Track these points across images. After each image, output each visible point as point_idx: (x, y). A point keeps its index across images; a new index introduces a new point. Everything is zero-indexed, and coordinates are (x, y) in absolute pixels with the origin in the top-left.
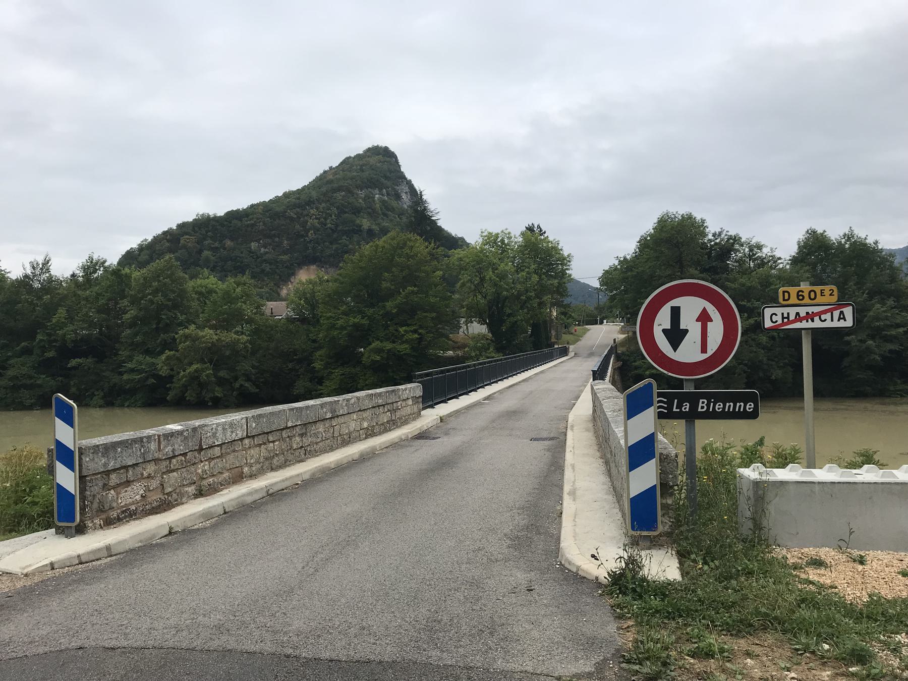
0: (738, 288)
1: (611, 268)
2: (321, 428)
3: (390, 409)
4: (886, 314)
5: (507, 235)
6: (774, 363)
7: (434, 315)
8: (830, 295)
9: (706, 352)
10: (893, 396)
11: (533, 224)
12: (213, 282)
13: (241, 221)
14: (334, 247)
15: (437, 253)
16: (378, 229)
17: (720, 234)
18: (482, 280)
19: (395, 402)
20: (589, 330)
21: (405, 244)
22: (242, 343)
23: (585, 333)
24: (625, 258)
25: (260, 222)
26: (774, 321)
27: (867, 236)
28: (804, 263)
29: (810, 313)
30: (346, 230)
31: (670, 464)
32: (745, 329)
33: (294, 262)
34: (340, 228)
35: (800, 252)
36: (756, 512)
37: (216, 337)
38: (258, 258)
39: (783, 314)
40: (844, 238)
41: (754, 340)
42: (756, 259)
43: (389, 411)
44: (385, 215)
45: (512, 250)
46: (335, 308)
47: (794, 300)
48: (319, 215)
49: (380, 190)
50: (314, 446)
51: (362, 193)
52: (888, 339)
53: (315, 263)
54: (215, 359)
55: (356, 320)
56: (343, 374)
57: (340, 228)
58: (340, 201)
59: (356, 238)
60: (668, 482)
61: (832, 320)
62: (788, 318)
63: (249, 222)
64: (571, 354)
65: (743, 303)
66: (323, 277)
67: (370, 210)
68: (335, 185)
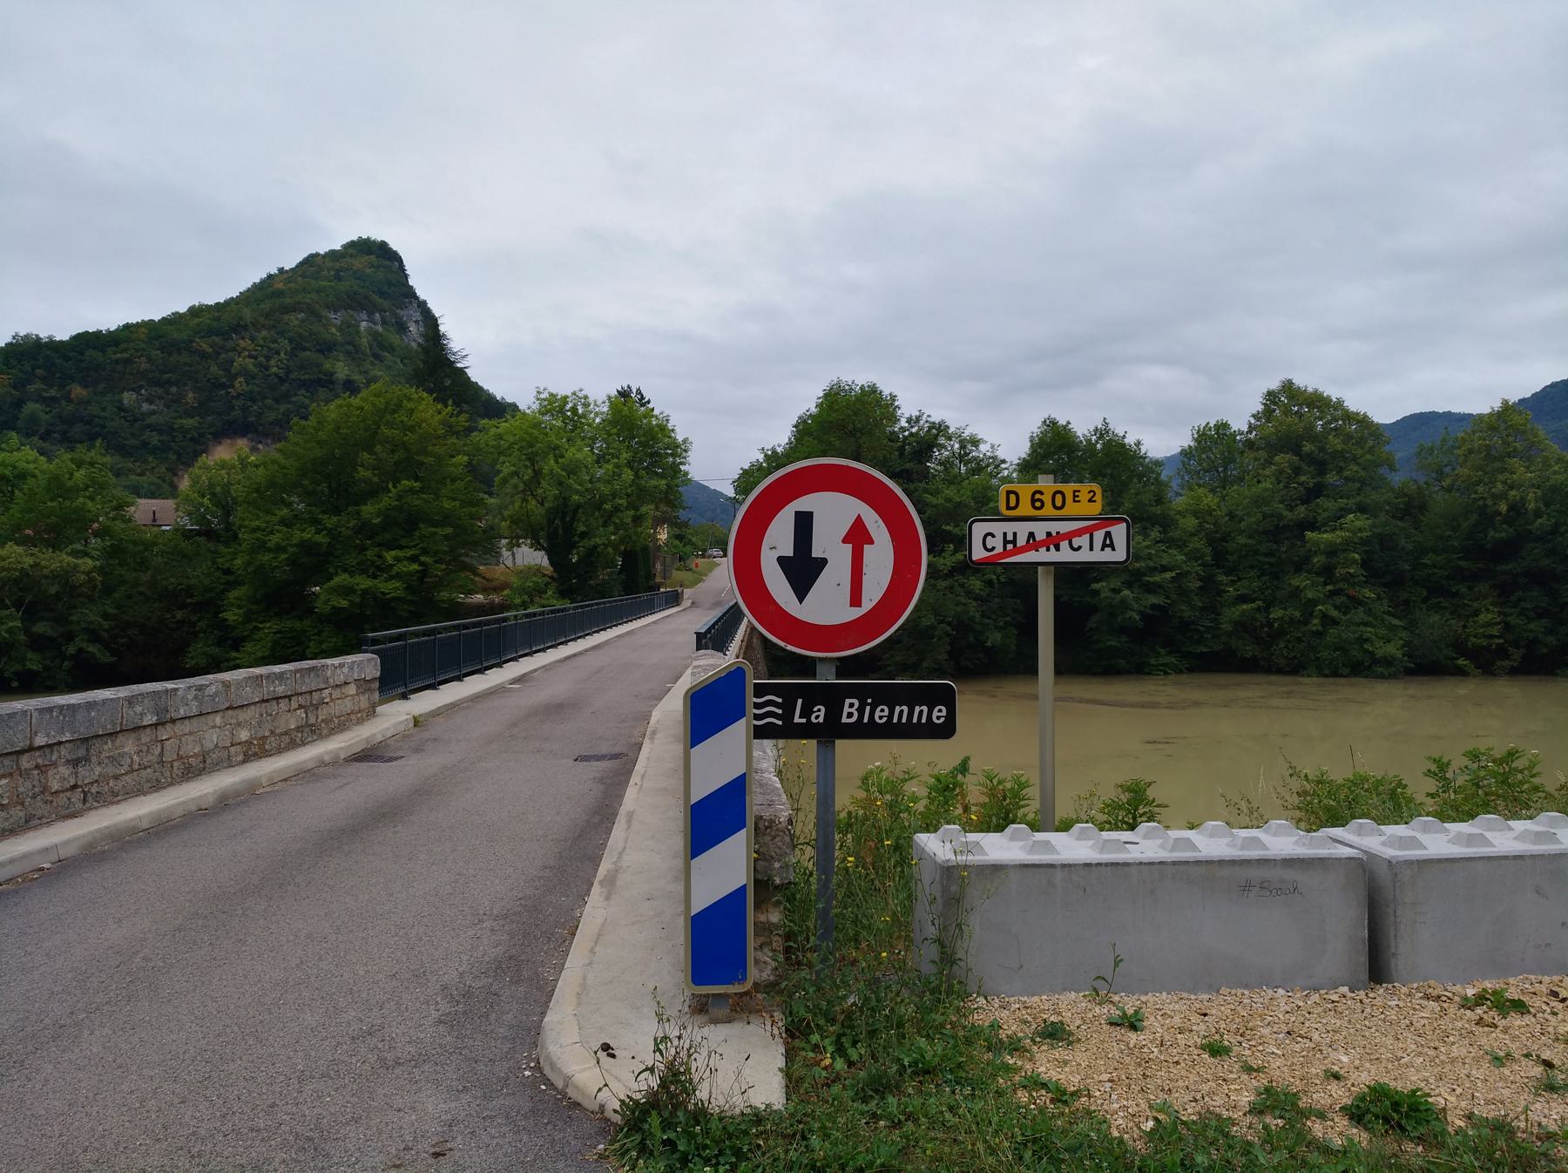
0: (942, 504)
1: (753, 465)
2: (129, 745)
3: (303, 703)
4: (1148, 551)
5: (583, 400)
6: (990, 621)
7: (449, 530)
8: (1090, 501)
9: (859, 605)
10: (1154, 673)
11: (629, 387)
12: (30, 458)
13: (104, 352)
14: (283, 408)
15: (457, 423)
16: (364, 381)
17: (918, 419)
18: (537, 474)
19: (315, 691)
20: (719, 565)
21: (399, 406)
22: (83, 572)
23: (710, 570)
24: (774, 452)
25: (142, 356)
26: (989, 547)
27: (1126, 432)
28: (1039, 469)
29: (1054, 534)
30: (305, 380)
31: (777, 840)
32: (950, 569)
33: (204, 430)
34: (294, 376)
35: (1033, 452)
36: (945, 928)
37: (30, 560)
38: (136, 420)
39: (1005, 534)
40: (1095, 434)
41: (962, 586)
42: (969, 461)
43: (301, 707)
44: (376, 356)
45: (589, 425)
46: (268, 512)
47: (1025, 509)
48: (256, 350)
49: (370, 314)
50: (108, 784)
51: (336, 318)
52: (1150, 589)
53: (247, 433)
54: (27, 601)
55: (306, 536)
56: (278, 632)
57: (294, 376)
58: (296, 329)
59: (323, 393)
60: (770, 878)
61: (1091, 549)
62: (1014, 542)
63: (118, 355)
64: (686, 603)
65: (948, 528)
66: (247, 457)
67: (350, 348)
68: (288, 301)
